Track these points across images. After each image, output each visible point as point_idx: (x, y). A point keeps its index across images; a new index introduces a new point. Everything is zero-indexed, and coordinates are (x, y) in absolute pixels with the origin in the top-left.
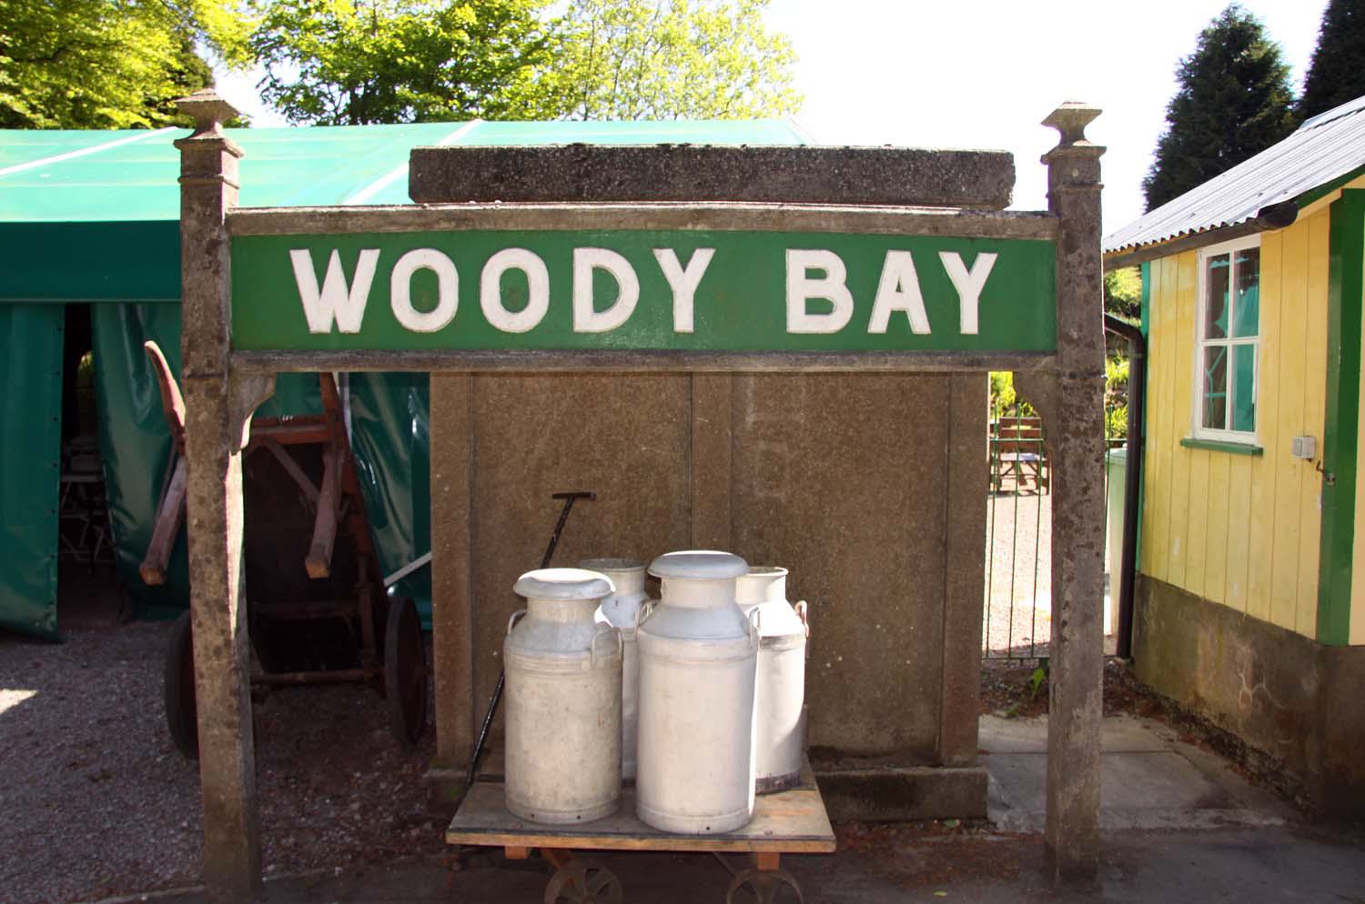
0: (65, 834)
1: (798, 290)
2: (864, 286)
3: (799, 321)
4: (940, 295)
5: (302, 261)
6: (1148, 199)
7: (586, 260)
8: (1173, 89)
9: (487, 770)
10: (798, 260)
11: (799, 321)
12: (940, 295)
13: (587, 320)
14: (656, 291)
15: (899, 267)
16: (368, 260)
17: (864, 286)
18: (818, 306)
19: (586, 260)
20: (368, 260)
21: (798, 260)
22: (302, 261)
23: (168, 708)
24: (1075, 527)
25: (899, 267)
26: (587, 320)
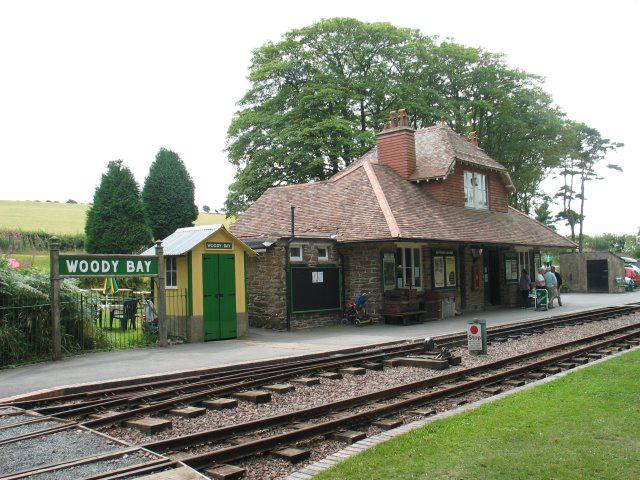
0: (313, 94)
1: (128, 266)
2: (136, 265)
3: (129, 271)
4: (144, 267)
5: (68, 262)
6: (103, 184)
7: (103, 262)
8: (98, 183)
9: (222, 239)
10: (128, 262)
11: (129, 271)
12: (144, 267)
13: (104, 270)
14: (112, 266)
15: (140, 263)
16: (76, 262)
17: (136, 265)
18: (131, 268)
19: (103, 262)
20: (76, 262)
21: (128, 262)
22: (68, 262)
23: (288, 294)
24: (469, 333)
25: (140, 263)
26: (104, 270)
